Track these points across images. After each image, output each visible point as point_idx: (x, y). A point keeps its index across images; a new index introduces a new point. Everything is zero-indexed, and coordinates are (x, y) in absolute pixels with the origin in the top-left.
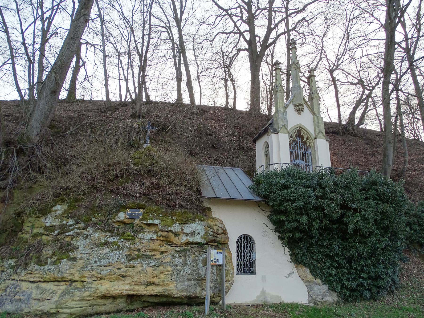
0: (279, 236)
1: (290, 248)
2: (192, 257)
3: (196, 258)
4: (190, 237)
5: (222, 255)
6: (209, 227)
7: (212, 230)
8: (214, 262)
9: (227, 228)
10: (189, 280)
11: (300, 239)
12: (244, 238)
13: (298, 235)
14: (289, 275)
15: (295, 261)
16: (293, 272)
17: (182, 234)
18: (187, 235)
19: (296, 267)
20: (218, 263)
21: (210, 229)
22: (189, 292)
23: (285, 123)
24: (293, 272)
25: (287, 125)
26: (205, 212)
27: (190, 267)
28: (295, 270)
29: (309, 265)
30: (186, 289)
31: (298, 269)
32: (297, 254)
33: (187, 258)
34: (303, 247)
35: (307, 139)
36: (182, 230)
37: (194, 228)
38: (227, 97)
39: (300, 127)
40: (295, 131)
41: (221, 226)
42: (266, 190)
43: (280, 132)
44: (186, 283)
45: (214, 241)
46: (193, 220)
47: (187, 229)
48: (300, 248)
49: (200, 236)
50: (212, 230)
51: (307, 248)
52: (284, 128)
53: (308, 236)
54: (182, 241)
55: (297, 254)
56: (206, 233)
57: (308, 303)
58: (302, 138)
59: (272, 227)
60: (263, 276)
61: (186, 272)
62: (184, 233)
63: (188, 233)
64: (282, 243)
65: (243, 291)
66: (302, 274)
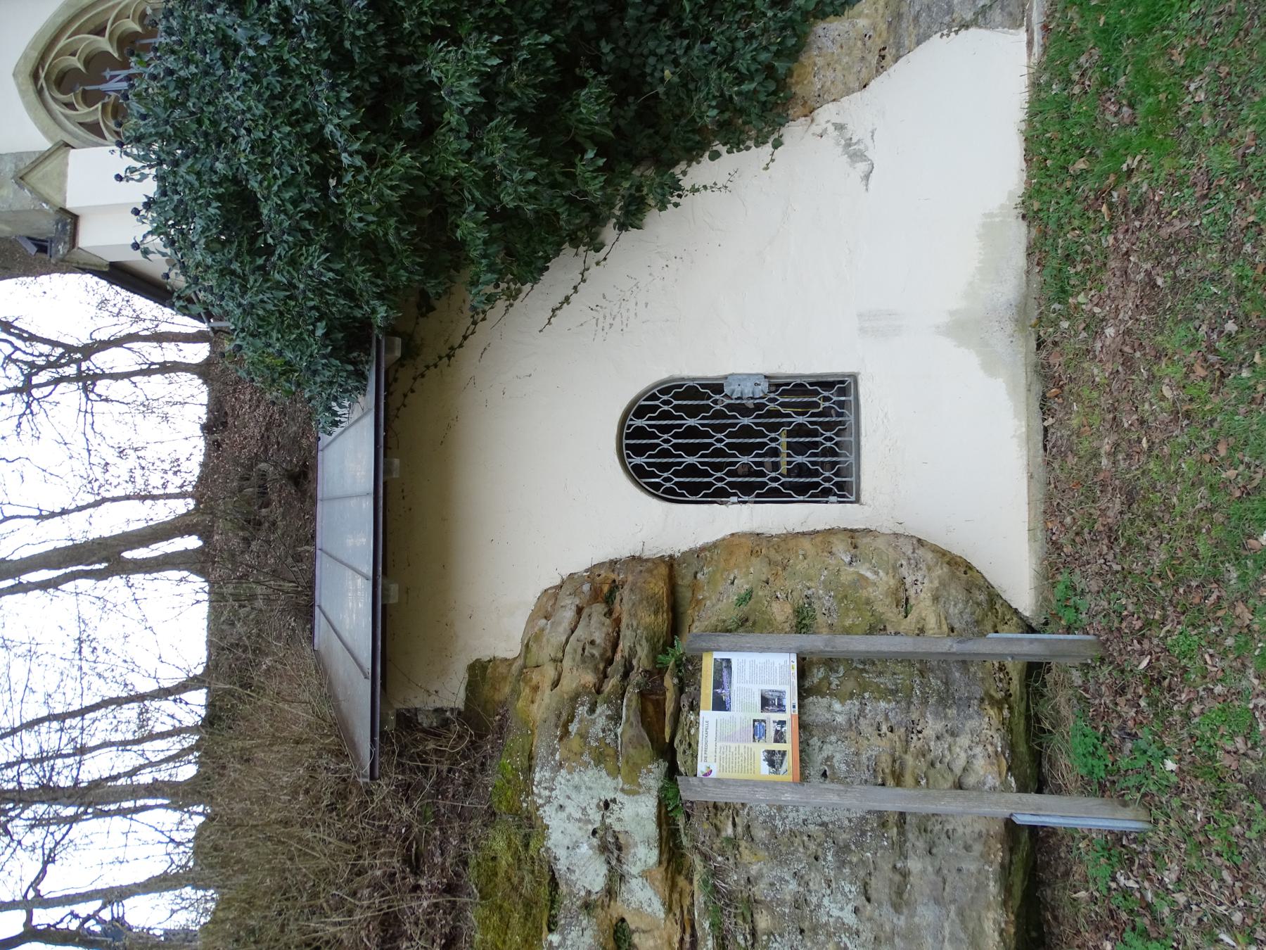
0: (622, 227)
1: (695, 149)
2: (755, 863)
3: (760, 834)
4: (627, 857)
5: (736, 658)
6: (566, 733)
7: (582, 710)
8: (779, 737)
9: (580, 559)
10: (900, 898)
11: (628, 84)
12: (639, 450)
13: (590, 105)
14: (855, 154)
15: (770, 116)
16: (840, 127)
17: (618, 909)
18: (616, 879)
19: (810, 112)
20: (791, 699)
21: (573, 728)
22: (981, 888)
23: (9, 168)
24: (840, 127)
25: (18, 156)
26: (483, 717)
27: (816, 882)
28: (827, 114)
29: (789, 24)
30: (961, 913)
31: (822, 98)
32: (725, 103)
33: (760, 890)
34: (676, 63)
35: (100, 31)
36: (587, 906)
37: (572, 828)
38: (166, 368)
39: (35, 76)
40: (56, 108)
41: (569, 615)
42: (300, 338)
43: (57, 199)
44: (926, 914)
45: (650, 699)
46: (530, 827)
47: (585, 872)
48: (688, 81)
49: (620, 797)
50: (582, 710)
51: (684, 35)
52: (34, 178)
53: (605, 32)
54: (658, 908)
55: (725, 103)
56: (599, 759)
57: (1022, 35)
58: (96, 61)
59: (564, 269)
60: (862, 330)
61: (850, 918)
62: (610, 892)
63: (604, 870)
64: (663, 207)
65: (955, 462)
66: (848, 68)
